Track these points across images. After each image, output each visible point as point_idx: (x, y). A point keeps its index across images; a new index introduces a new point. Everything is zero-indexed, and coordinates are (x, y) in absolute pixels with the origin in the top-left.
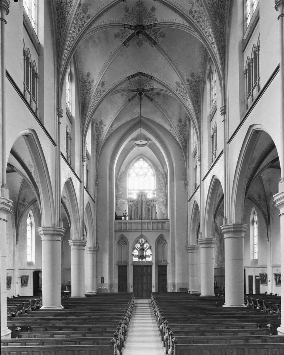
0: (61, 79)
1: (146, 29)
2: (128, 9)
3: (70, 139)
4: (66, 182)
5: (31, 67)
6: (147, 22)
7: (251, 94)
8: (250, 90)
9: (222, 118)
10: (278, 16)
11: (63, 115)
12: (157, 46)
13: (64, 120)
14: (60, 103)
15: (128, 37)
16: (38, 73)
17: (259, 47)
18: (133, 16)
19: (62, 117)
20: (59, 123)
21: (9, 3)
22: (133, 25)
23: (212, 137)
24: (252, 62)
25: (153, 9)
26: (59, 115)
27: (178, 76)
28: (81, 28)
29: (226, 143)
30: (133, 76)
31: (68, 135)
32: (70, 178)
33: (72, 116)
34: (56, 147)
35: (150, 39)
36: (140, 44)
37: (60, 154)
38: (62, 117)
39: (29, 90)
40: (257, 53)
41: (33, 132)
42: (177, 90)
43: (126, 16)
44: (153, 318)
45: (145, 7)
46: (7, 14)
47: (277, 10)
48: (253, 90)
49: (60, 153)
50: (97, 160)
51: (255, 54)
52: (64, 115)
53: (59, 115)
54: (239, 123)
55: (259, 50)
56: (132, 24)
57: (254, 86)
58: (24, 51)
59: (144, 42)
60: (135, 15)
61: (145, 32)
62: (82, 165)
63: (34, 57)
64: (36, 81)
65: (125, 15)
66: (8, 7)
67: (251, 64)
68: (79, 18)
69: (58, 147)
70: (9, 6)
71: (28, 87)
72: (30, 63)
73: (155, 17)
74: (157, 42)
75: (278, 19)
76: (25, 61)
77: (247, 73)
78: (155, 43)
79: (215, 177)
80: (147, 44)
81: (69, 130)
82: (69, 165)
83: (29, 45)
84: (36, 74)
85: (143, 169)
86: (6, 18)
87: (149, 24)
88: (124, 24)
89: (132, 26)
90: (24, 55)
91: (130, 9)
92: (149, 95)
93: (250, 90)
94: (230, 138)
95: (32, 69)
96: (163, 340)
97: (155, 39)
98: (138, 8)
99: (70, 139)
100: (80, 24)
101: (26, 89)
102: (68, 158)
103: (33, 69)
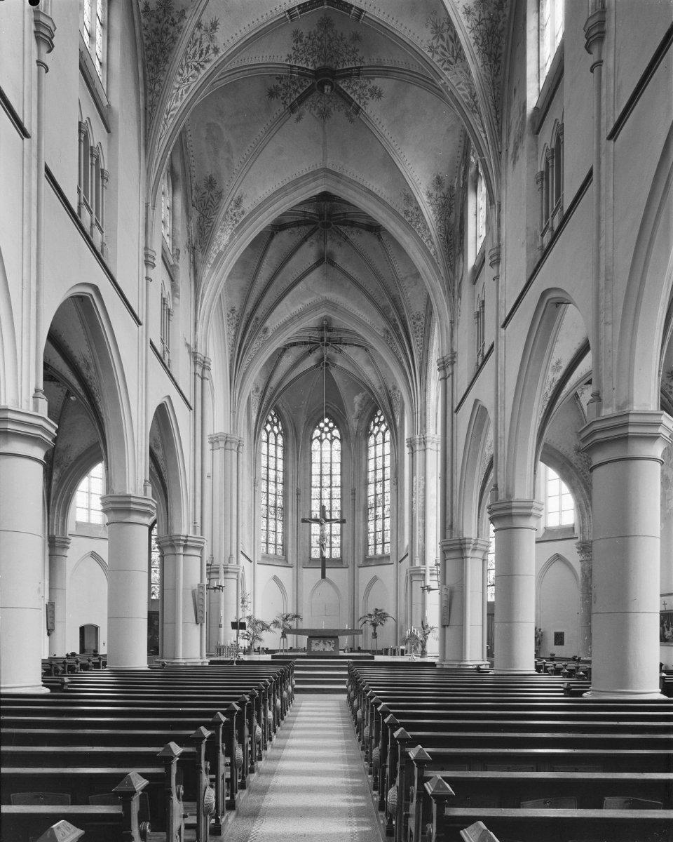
0: (152, 184)
1: (340, 77)
2: (301, 36)
3: (169, 314)
4: (160, 405)
5: (92, 155)
7: (550, 226)
8: (547, 217)
10: (592, 65)
15: (298, 95)
16: (106, 169)
18: (312, 49)
19: (154, 266)
21: (53, 29)
22: (310, 68)
23: (478, 317)
24: (552, 158)
31: (164, 304)
33: (109, 106)
37: (149, 344)
38: (154, 266)
39: (89, 204)
40: (561, 138)
41: (93, 289)
42: (406, 213)
43: (296, 50)
44: (345, 719)
46: (49, 51)
47: (590, 53)
48: (552, 216)
49: (149, 342)
56: (308, 65)
57: (555, 207)
58: (80, 123)
59: (334, 110)
61: (337, 85)
62: (193, 371)
63: (97, 135)
64: (103, 186)
65: (293, 48)
66: (52, 38)
67: (550, 162)
71: (87, 197)
72: (92, 147)
74: (363, 108)
75: (592, 71)
76: (82, 144)
77: (542, 179)
79: (479, 403)
81: (167, 293)
82: (166, 367)
83: (90, 112)
84: (102, 170)
86: (47, 58)
88: (290, 66)
89: (308, 70)
90: (80, 131)
91: (306, 34)
93: (547, 217)
94: (507, 315)
95: (94, 159)
96: (382, 806)
99: (167, 313)
101: (82, 201)
102: (164, 354)
103: (98, 161)
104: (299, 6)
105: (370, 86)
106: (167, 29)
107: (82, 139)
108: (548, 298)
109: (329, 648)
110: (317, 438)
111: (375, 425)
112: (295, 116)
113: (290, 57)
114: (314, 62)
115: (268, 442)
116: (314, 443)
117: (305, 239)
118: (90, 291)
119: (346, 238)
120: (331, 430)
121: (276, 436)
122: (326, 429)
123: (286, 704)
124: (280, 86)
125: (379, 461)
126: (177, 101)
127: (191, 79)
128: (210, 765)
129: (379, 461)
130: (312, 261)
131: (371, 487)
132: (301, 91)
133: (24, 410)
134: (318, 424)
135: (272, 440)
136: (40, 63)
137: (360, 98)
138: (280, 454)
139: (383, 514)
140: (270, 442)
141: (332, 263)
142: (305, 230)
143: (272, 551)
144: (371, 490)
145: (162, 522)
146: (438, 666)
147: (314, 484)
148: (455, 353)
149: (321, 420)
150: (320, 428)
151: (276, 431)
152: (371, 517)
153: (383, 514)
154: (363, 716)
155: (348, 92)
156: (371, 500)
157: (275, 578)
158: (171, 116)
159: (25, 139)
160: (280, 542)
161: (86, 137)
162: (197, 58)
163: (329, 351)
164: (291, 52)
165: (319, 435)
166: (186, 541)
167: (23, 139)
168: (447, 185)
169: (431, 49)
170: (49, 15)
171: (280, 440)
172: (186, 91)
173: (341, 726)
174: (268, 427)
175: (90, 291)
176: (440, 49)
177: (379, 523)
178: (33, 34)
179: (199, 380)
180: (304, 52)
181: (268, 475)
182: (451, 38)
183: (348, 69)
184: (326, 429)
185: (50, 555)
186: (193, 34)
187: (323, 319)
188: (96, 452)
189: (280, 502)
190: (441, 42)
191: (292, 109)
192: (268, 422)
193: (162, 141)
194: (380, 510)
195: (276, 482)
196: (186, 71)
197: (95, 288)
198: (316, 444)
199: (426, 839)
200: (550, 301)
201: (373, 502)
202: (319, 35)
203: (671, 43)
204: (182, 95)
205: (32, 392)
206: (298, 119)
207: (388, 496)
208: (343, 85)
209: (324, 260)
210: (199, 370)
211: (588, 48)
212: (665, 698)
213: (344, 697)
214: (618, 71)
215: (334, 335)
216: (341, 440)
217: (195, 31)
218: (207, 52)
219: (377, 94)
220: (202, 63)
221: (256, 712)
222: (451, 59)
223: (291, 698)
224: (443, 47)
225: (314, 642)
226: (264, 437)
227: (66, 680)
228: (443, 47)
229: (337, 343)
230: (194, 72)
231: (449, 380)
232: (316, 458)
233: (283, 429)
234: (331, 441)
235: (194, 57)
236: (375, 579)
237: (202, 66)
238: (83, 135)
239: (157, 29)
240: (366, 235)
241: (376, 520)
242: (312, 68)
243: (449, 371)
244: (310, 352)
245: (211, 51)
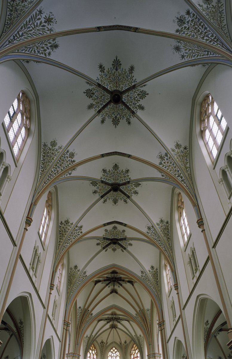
6: (124, 86)
9: (176, 292)
11: (54, 288)
12: (131, 157)
13: (54, 292)
14: (53, 280)
28: (66, 167)
30: (109, 224)
32: (52, 336)
34: (45, 309)
36: (114, 250)
45: (123, 69)
50: (85, 353)
52: (55, 288)
54: (189, 294)
60: (111, 79)
63: (40, 250)
68: (65, 160)
69: (46, 310)
78: (125, 249)
79: (177, 338)
80: (119, 250)
85: (124, 98)
86: (28, 228)
90: (34, 249)
92: (126, 192)
100: (65, 164)
106: (67, 227)
107: (35, 251)
108: (200, 298)
110: (110, 356)
111: (133, 350)
117: (107, 285)
120: (116, 352)
122: (114, 352)
126: (68, 244)
127: (73, 239)
134: (110, 350)
140: (91, 357)
141: (116, 292)
142: (107, 282)
148: (164, 321)
149: (112, 349)
150: (111, 352)
155: (122, 244)
162: (75, 234)
163: (116, 323)
164: (104, 234)
165: (111, 354)
167: (14, 246)
168: (155, 268)
169: (149, 271)
172: (71, 242)
174: (91, 351)
175: (28, 296)
179: (65, 331)
184: (114, 352)
190: (150, 231)
192: (90, 349)
193: (61, 254)
197: (30, 294)
199: (94, 358)
200: (201, 299)
203: (231, 215)
204: (69, 243)
206: (106, 251)
211: (199, 227)
219: (131, 245)
226: (89, 355)
231: (163, 331)
234: (116, 357)
237: (77, 236)
240: (129, 284)
244: (108, 322)
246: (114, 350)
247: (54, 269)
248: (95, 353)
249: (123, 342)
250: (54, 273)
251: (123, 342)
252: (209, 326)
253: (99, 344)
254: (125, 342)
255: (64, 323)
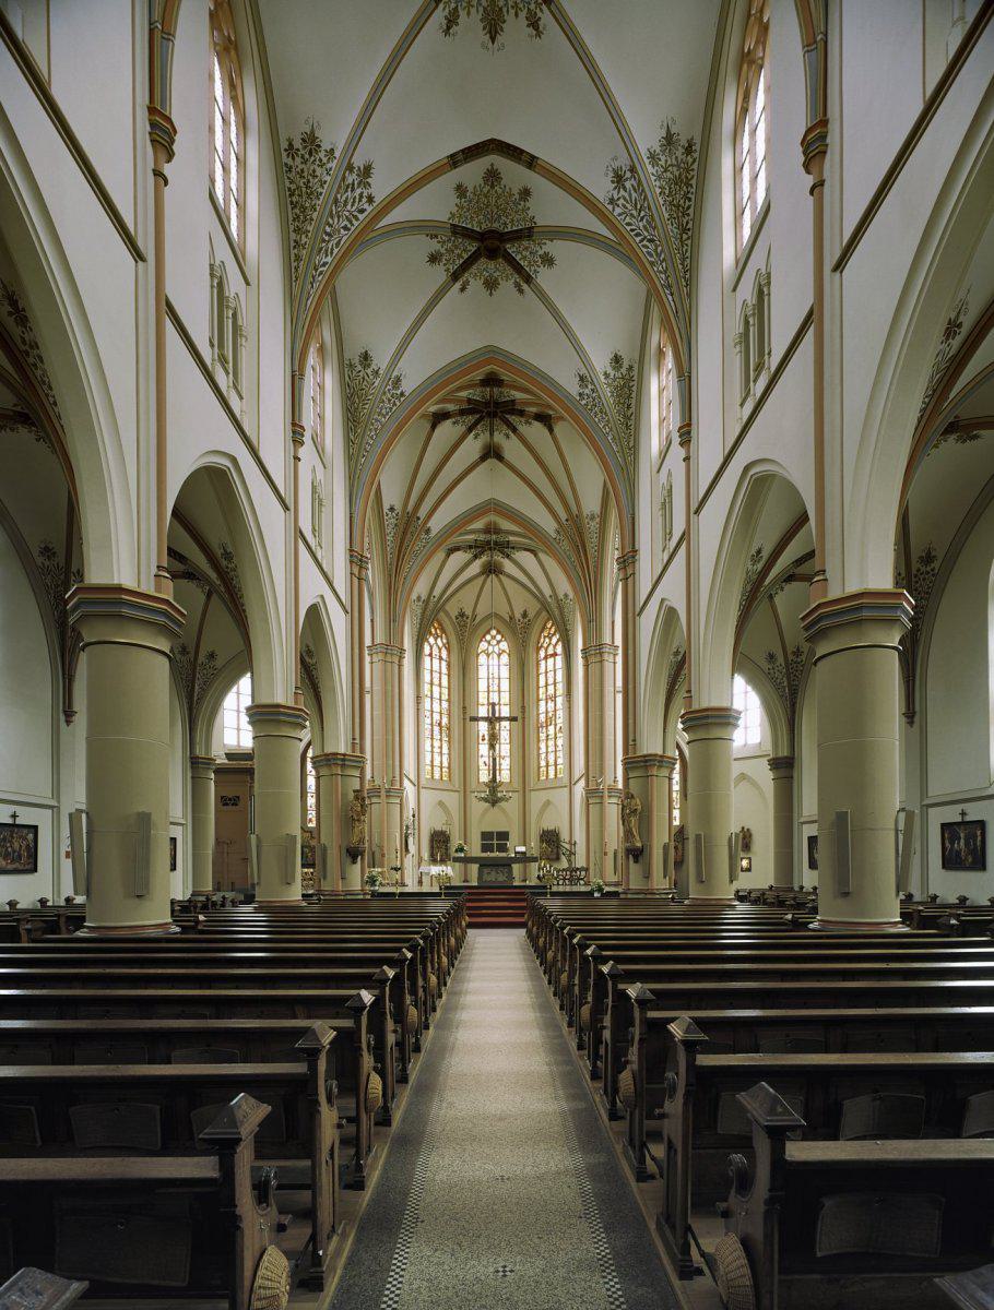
7: (752, 392)
17: (769, 275)
19: (302, 444)
20: (297, 459)
25: (526, 193)
26: (297, 440)
27: (615, 123)
29: (827, 268)
35: (518, 269)
40: (765, 289)
47: (808, 172)
51: (761, 294)
52: (307, 438)
53: (297, 440)
55: (769, 283)
58: (212, 266)
70: (173, 141)
73: (530, 213)
79: (666, 603)
80: (507, 286)
83: (224, 254)
86: (167, 169)
87: (515, 228)
90: (212, 275)
91: (470, 189)
94: (700, 498)
97: (527, 269)
98: (488, 188)
104: (463, 151)
105: (541, 252)
106: (314, 171)
109: (501, 878)
111: (545, 637)
112: (458, 285)
113: (453, 215)
114: (480, 223)
115: (431, 655)
116: (480, 657)
117: (470, 430)
118: (227, 462)
119: (514, 430)
120: (499, 642)
121: (440, 650)
123: (460, 941)
124: (443, 251)
125: (551, 675)
126: (327, 256)
128: (375, 1040)
129: (551, 675)
130: (476, 456)
131: (542, 703)
132: (466, 256)
133: (143, 589)
134: (484, 636)
135: (435, 651)
136: (158, 174)
137: (530, 265)
138: (444, 670)
139: (555, 734)
141: (500, 458)
142: (471, 419)
143: (437, 776)
144: (542, 709)
145: (317, 742)
146: (622, 896)
147: (481, 701)
149: (488, 632)
151: (441, 645)
152: (543, 736)
153: (555, 734)
154: (555, 957)
156: (542, 718)
157: (441, 803)
158: (321, 273)
159: (140, 263)
160: (445, 764)
161: (220, 285)
162: (349, 207)
163: (498, 558)
166: (343, 760)
167: (136, 262)
168: (626, 365)
170: (167, 114)
171: (444, 654)
173: (520, 966)
176: (621, 201)
177: (551, 743)
178: (148, 136)
179: (356, 580)
180: (468, 210)
181: (432, 691)
182: (634, 189)
183: (516, 231)
184: (494, 642)
185: (193, 778)
186: (344, 179)
187: (489, 524)
188: (244, 660)
189: (445, 721)
191: (455, 277)
192: (431, 634)
194: (551, 728)
195: (440, 700)
196: (336, 220)
197: (234, 460)
198: (482, 659)
201: (544, 720)
202: (485, 190)
205: (154, 570)
207: (560, 713)
208: (511, 249)
209: (492, 453)
210: (356, 571)
211: (807, 167)
212: (906, 930)
213: (523, 932)
214: (746, 335)
215: (501, 538)
216: (509, 655)
217: (347, 174)
218: (360, 201)
219: (548, 261)
220: (355, 213)
221: (429, 955)
222: (634, 212)
223: (464, 934)
224: (625, 199)
225: (486, 871)
227: (201, 918)
228: (625, 199)
229: (505, 548)
230: (346, 222)
232: (483, 672)
233: (448, 643)
234: (499, 655)
235: (345, 205)
236: (548, 803)
238: (216, 281)
239: (302, 171)
240: (537, 425)
241: (547, 740)
242: (478, 229)
243: (629, 572)
244: (476, 557)
245: (364, 200)
246: (493, 637)
247: (296, 368)
248: (444, 645)
249: (518, 615)
250: (297, 378)
251: (518, 615)
252: (759, 566)
253: (454, 618)
254: (525, 615)
255: (351, 556)
